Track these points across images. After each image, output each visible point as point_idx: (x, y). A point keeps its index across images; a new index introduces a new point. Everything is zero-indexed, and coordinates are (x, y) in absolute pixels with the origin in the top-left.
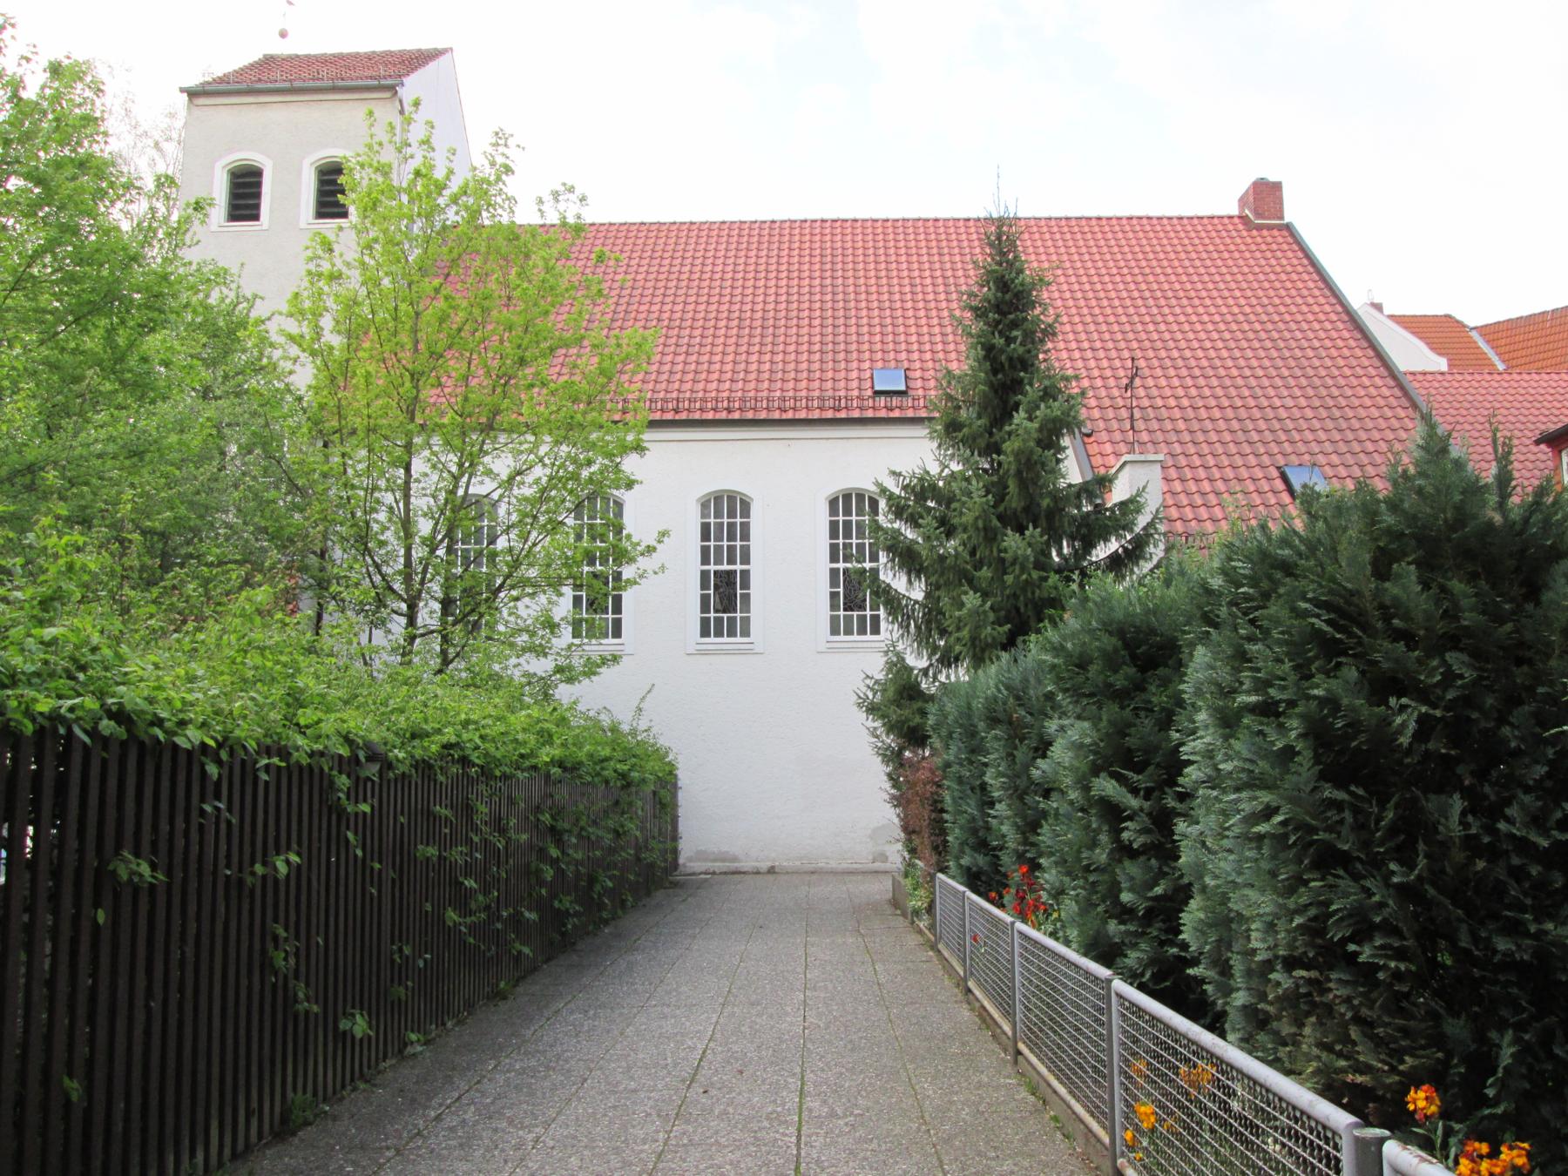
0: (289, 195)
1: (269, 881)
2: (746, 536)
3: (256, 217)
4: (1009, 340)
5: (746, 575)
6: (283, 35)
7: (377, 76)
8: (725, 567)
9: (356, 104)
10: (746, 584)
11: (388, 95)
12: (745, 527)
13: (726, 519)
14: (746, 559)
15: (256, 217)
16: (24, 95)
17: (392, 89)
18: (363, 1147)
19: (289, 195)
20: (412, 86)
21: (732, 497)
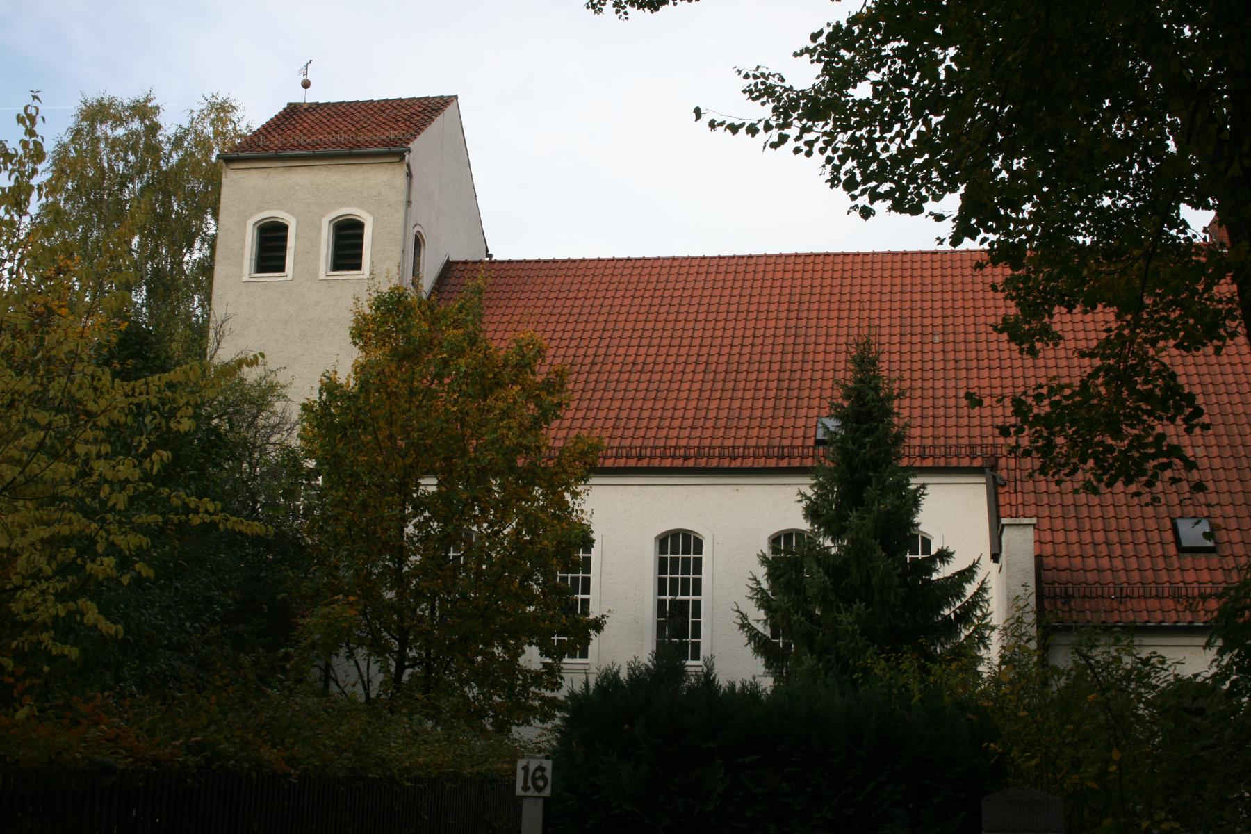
0: (309, 247)
1: (1029, 199)
2: (698, 570)
3: (281, 268)
4: (862, 446)
5: (697, 604)
6: (306, 85)
7: (389, 131)
8: (680, 597)
9: (369, 167)
10: (697, 613)
11: (396, 159)
12: (698, 562)
13: (679, 553)
14: (698, 591)
15: (283, 270)
16: (245, 369)
17: (401, 156)
18: (560, 405)
19: (309, 247)
20: (420, 147)
21: (687, 534)
